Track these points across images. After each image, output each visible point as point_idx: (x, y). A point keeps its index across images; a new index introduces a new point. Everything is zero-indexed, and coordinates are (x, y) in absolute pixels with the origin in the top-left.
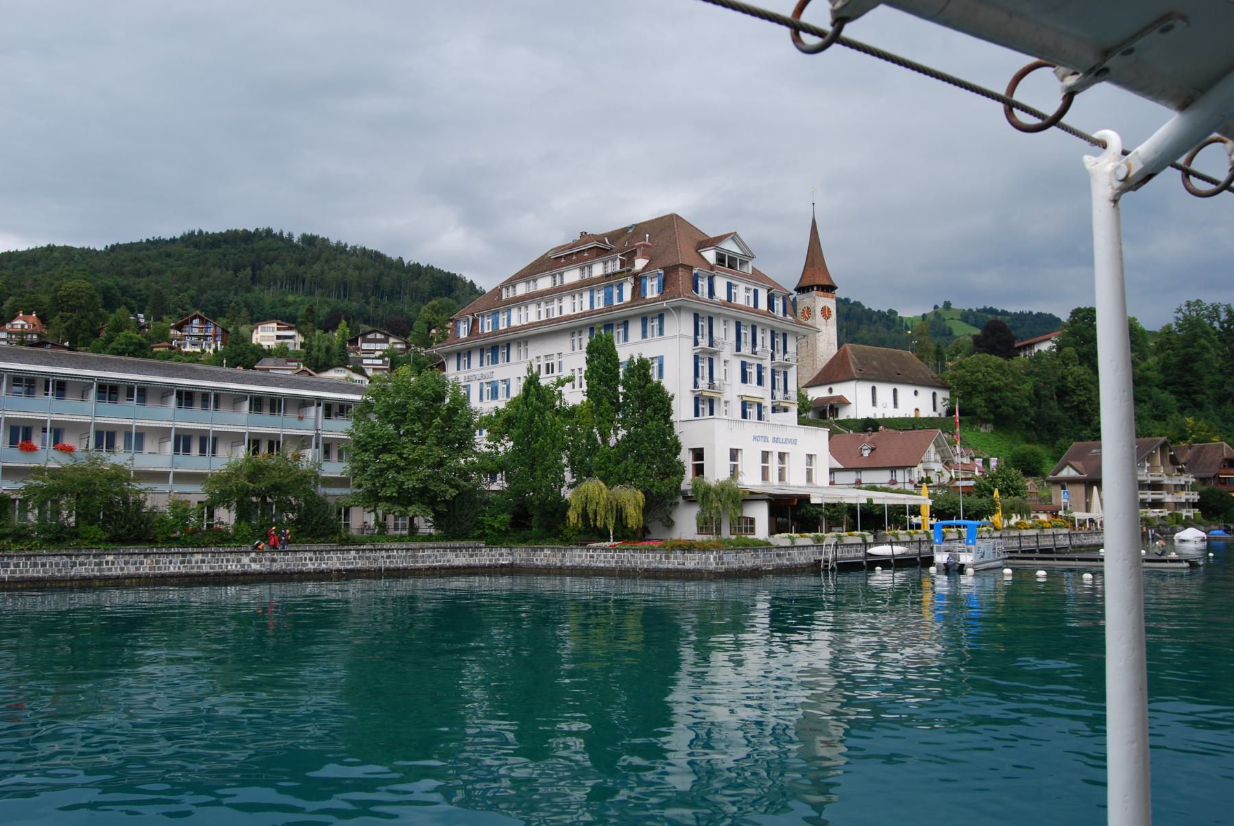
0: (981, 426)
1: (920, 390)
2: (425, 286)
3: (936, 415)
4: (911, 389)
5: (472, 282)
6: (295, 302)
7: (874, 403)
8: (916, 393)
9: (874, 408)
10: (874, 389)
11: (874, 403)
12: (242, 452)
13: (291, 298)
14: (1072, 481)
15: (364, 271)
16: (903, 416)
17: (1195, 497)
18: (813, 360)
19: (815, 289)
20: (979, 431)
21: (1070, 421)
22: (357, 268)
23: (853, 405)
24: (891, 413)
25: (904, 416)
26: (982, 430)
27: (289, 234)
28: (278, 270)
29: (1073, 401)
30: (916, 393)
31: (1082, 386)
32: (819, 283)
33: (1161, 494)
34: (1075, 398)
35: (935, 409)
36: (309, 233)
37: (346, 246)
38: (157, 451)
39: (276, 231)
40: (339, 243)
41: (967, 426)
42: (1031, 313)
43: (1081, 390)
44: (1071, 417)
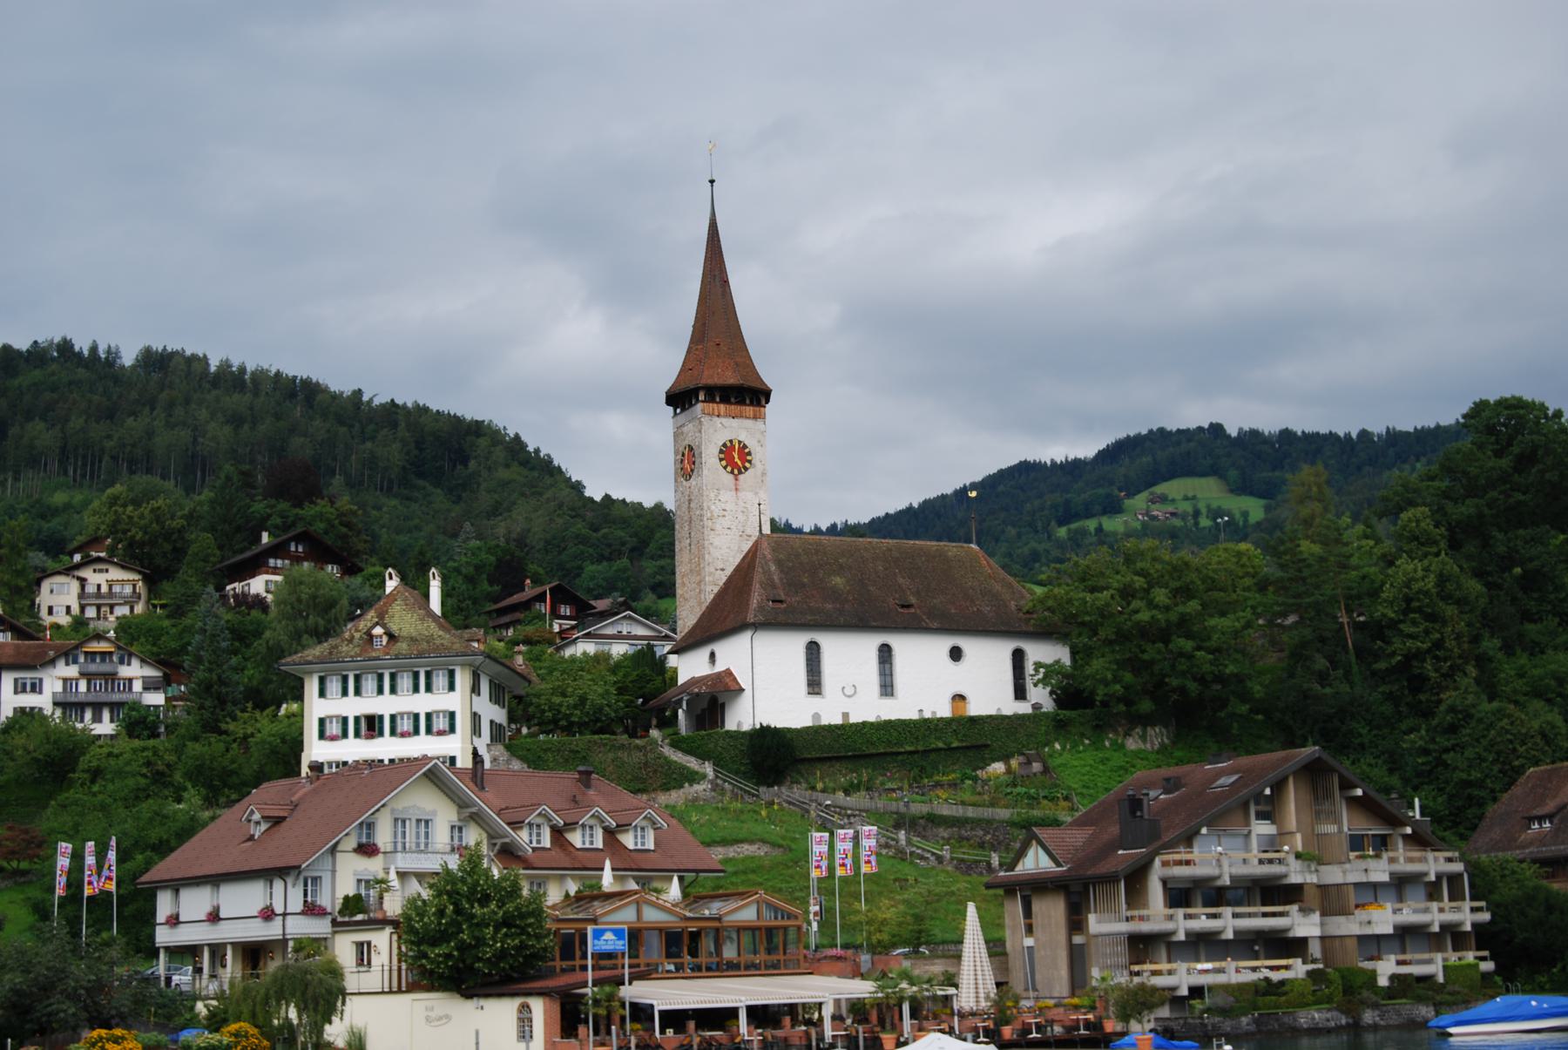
0: (1127, 734)
1: (969, 645)
2: (393, 453)
3: (1024, 708)
4: (940, 646)
5: (517, 437)
6: (67, 507)
7: (814, 684)
8: (956, 654)
9: (815, 699)
10: (813, 651)
11: (814, 684)
12: (232, 969)
13: (59, 498)
14: (1037, 886)
15: (246, 427)
16: (913, 715)
17: (1466, 915)
18: (699, 583)
19: (701, 397)
20: (1122, 746)
21: (1387, 709)
22: (236, 420)
23: (747, 694)
24: (869, 708)
25: (915, 716)
26: (1132, 744)
27: (109, 351)
28: (41, 434)
29: (1394, 654)
30: (956, 654)
31: (1419, 610)
32: (710, 382)
33: (1281, 914)
34: (1397, 644)
35: (1020, 693)
36: (157, 346)
37: (242, 370)
38: (1376, 954)
39: (82, 344)
40: (225, 365)
41: (1083, 735)
42: (1217, 429)
43: (1414, 623)
44: (1389, 696)
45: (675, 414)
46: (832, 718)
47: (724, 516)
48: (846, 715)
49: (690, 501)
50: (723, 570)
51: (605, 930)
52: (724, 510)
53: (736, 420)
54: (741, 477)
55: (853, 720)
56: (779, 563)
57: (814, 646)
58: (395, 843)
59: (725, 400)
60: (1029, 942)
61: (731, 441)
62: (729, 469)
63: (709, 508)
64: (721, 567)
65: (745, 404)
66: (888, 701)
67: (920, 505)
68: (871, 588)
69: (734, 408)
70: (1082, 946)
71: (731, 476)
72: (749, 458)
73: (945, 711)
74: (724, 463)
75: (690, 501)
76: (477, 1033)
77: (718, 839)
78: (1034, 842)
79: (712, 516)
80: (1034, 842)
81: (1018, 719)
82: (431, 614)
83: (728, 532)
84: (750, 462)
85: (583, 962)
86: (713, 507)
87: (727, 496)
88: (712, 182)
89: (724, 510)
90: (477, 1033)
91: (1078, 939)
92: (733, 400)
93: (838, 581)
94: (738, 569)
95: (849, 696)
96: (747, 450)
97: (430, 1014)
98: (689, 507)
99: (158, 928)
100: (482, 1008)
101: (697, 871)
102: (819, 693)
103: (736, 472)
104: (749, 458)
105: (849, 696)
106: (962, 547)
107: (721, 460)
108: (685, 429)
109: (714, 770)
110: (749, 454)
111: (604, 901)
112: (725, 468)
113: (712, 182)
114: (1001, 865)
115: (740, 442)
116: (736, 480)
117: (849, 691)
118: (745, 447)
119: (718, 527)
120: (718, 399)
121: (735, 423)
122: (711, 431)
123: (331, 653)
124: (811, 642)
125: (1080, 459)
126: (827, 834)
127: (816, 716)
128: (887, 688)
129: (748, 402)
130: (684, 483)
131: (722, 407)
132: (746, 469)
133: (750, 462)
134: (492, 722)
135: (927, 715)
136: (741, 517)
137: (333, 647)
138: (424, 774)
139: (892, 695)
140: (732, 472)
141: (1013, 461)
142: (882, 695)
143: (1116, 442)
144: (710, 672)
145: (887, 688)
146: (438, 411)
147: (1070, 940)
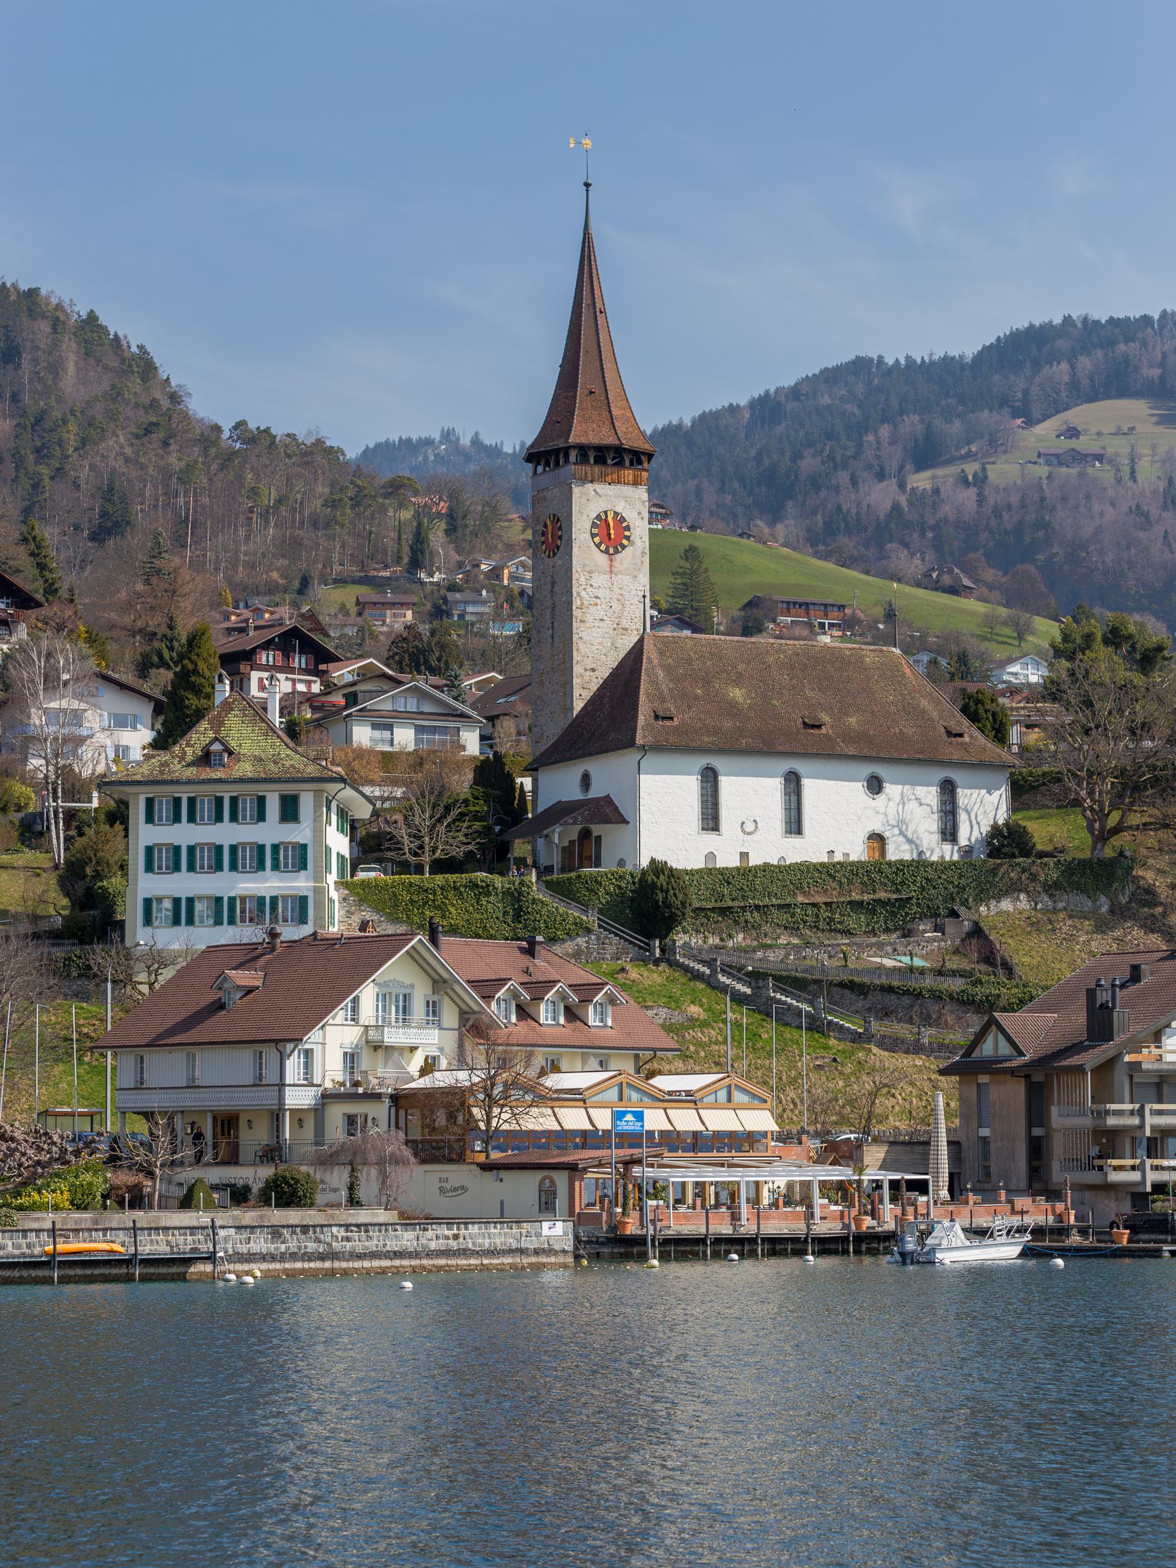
7: (711, 820)
9: (711, 837)
32: (584, 440)
45: (535, 472)
46: (728, 860)
47: (596, 605)
48: (744, 856)
49: (553, 584)
50: (593, 670)
51: (628, 1112)
52: (597, 597)
53: (612, 487)
54: (618, 557)
55: (754, 861)
56: (668, 669)
57: (711, 774)
58: (377, 1017)
59: (600, 460)
60: (985, 1132)
61: (606, 513)
62: (603, 547)
63: (579, 595)
64: (593, 666)
66: (795, 841)
67: (694, 421)
68: (775, 702)
70: (1039, 1138)
71: (606, 556)
72: (627, 533)
74: (597, 540)
75: (553, 584)
76: (502, 1203)
78: (994, 1027)
79: (582, 604)
80: (994, 1027)
81: (943, 867)
82: (271, 728)
83: (601, 624)
84: (628, 538)
85: (626, 1145)
86: (583, 594)
87: (599, 580)
88: (587, 185)
89: (597, 597)
90: (502, 1203)
91: (1037, 1132)
93: (736, 693)
94: (616, 673)
96: (624, 525)
97: (444, 1185)
98: (552, 591)
99: (567, 1127)
100: (501, 1180)
101: (655, 1050)
103: (611, 550)
104: (627, 533)
105: (749, 834)
106: (882, 651)
107: (593, 536)
108: (549, 494)
109: (599, 919)
110: (628, 528)
112: (598, 546)
113: (587, 185)
114: (221, 755)
115: (616, 514)
116: (611, 560)
117: (750, 827)
118: (623, 519)
119: (589, 618)
120: (592, 461)
123: (162, 772)
125: (953, 358)
127: (711, 856)
128: (795, 825)
129: (627, 463)
130: (546, 559)
132: (624, 547)
133: (628, 538)
134: (338, 854)
135: (838, 857)
136: (617, 607)
137: (162, 765)
138: (407, 952)
140: (606, 552)
141: (846, 356)
142: (786, 832)
143: (1012, 333)
144: (582, 797)
145: (795, 825)
147: (1029, 1131)
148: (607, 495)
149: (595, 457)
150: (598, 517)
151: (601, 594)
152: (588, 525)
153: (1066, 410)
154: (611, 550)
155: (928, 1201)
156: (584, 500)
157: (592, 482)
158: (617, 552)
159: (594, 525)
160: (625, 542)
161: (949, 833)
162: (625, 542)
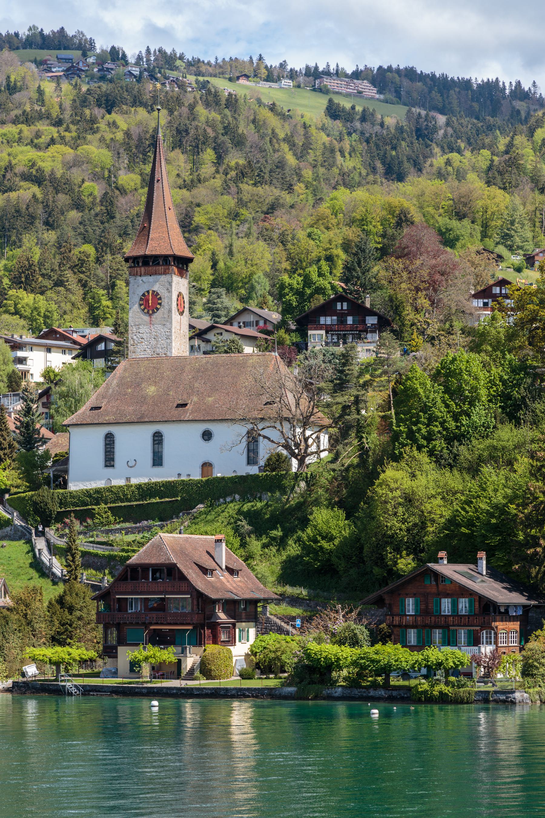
8: (207, 436)
48: (206, 466)
53: (152, 277)
62: (146, 311)
65: (158, 264)
66: (157, 469)
69: (151, 269)
73: (197, 476)
77: (49, 581)
92: (151, 264)
95: (131, 467)
102: (113, 466)
103: (151, 312)
104: (159, 301)
105: (131, 467)
110: (160, 299)
111: (33, 693)
115: (154, 291)
118: (158, 294)
120: (140, 264)
121: (151, 279)
122: (136, 286)
124: (156, 433)
126: (392, 683)
129: (161, 263)
131: (143, 269)
132: (158, 309)
133: (160, 304)
135: (184, 478)
136: (153, 342)
139: (106, 466)
140: (148, 312)
146: (380, 68)
148: (149, 282)
149: (143, 262)
150: (144, 295)
151: (144, 336)
152: (137, 299)
153: (273, 82)
154: (151, 312)
155: (388, 593)
156: (136, 286)
157: (140, 276)
158: (154, 312)
159: (141, 299)
160: (158, 306)
161: (251, 460)
162: (158, 306)
